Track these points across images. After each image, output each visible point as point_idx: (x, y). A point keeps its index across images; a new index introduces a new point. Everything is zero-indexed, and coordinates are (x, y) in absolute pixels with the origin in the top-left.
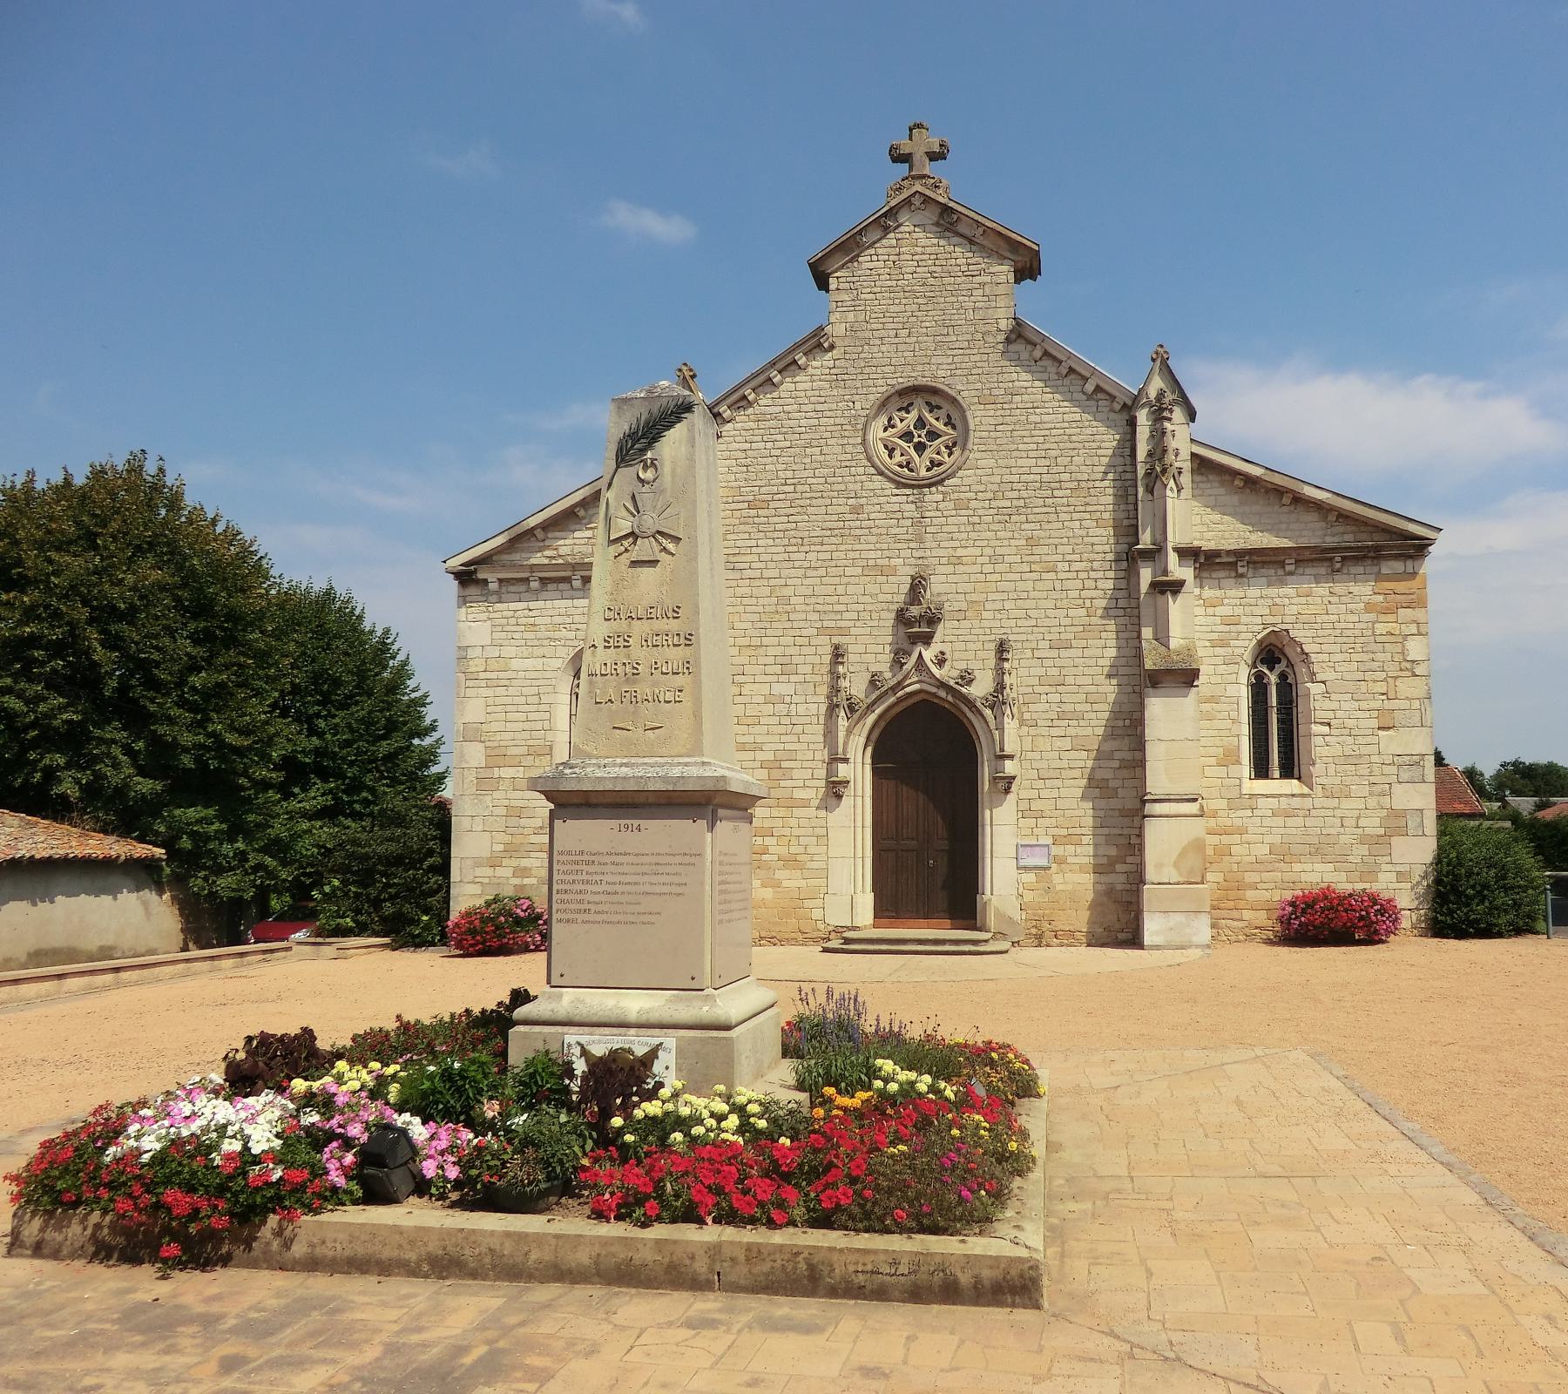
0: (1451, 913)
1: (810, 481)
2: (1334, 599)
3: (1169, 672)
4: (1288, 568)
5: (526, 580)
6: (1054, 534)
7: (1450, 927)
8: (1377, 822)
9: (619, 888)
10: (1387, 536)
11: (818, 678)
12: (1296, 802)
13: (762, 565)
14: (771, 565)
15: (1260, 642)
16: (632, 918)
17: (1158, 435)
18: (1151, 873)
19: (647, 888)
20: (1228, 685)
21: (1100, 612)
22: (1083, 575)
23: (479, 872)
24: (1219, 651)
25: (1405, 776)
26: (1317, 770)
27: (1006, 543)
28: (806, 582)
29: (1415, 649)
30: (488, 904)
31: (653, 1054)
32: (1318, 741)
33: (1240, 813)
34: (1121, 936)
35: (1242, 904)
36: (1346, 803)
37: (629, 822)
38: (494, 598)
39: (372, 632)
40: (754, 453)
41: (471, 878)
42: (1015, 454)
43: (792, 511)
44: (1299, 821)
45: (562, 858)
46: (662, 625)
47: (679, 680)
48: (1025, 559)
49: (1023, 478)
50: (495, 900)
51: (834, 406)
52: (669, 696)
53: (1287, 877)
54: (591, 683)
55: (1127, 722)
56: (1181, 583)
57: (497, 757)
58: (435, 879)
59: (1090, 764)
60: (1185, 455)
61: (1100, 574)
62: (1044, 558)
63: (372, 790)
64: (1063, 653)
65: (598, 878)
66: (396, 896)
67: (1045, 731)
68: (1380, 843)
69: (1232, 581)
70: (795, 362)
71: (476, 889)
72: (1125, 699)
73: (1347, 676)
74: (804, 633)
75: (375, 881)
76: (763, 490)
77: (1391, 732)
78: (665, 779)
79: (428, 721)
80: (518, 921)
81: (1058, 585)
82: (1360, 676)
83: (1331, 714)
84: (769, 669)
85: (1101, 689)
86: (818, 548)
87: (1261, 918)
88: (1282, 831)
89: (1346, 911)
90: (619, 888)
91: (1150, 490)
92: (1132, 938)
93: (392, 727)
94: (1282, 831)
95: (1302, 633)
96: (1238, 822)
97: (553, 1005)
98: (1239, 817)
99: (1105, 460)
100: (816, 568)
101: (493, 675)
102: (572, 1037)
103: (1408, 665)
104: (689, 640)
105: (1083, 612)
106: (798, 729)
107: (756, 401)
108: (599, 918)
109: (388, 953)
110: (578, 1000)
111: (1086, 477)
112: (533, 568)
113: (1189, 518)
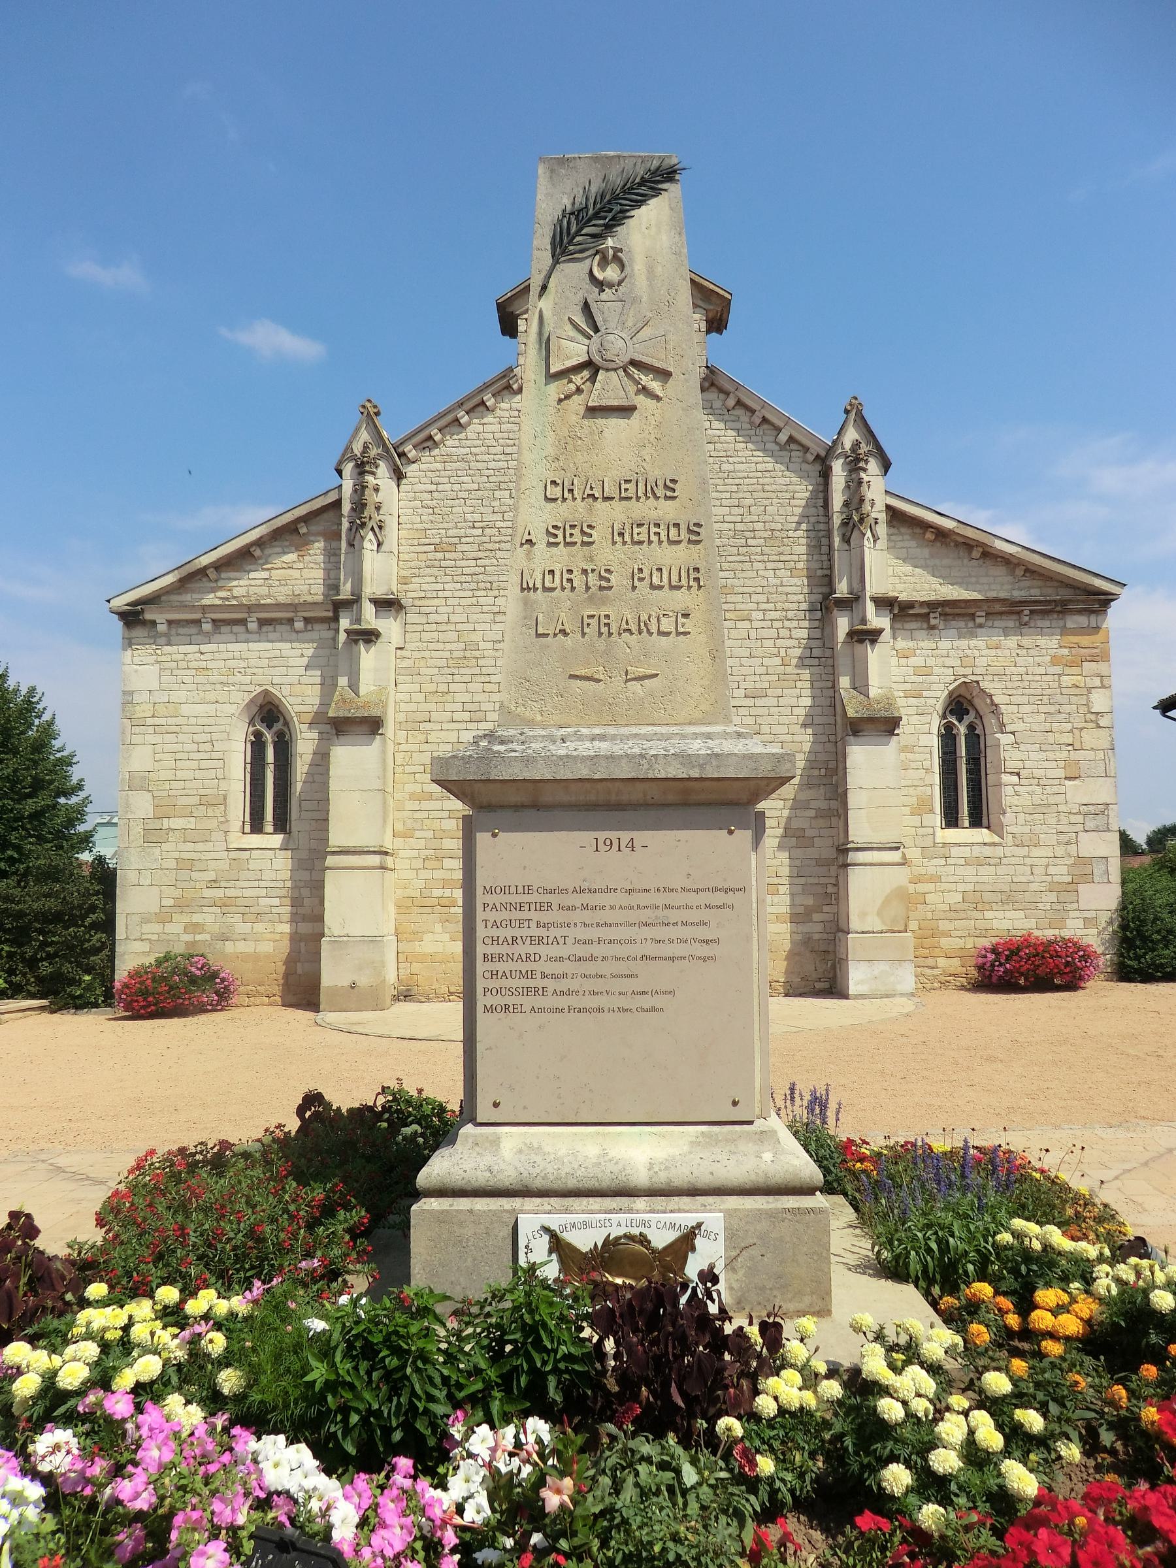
0: (1137, 958)
1: (499, 524)
2: (1023, 652)
3: (871, 720)
4: (979, 620)
5: (198, 622)
7: (1136, 971)
8: (1064, 870)
9: (597, 950)
10: (1072, 591)
12: (988, 851)
13: (450, 609)
14: (458, 609)
15: (951, 693)
17: (855, 485)
18: (855, 923)
19: (651, 949)
20: (922, 733)
21: (794, 661)
22: (777, 624)
23: (147, 928)
24: (912, 701)
25: (1090, 825)
26: (1007, 819)
28: (495, 627)
29: (1099, 701)
30: (159, 963)
31: (687, 1242)
32: (1009, 790)
33: (935, 862)
34: (819, 985)
35: (937, 952)
36: (1036, 852)
37: (613, 835)
38: (163, 640)
39: (16, 691)
40: (441, 495)
41: (137, 935)
43: (481, 554)
44: (992, 869)
45: (490, 899)
47: (681, 599)
50: (167, 958)
53: (981, 924)
55: (823, 772)
56: (879, 632)
57: (165, 808)
58: (98, 937)
59: (786, 813)
60: (880, 506)
61: (795, 624)
62: (739, 607)
63: (18, 848)
66: (56, 955)
69: (924, 632)
70: (483, 403)
71: (144, 947)
72: (820, 748)
73: (1035, 727)
74: (493, 679)
75: (31, 939)
76: (450, 533)
77: (1077, 782)
78: (684, 758)
79: (74, 781)
80: (193, 980)
81: (753, 633)
82: (1048, 727)
84: (456, 716)
85: (796, 738)
87: (954, 965)
88: (975, 879)
89: (1051, 957)
90: (597, 950)
91: (846, 540)
92: (831, 986)
93: (38, 785)
94: (975, 879)
95: (992, 685)
96: (932, 870)
97: (488, 1159)
98: (934, 866)
99: (798, 511)
102: (533, 1219)
103: (1093, 717)
105: (778, 661)
107: (442, 441)
108: (563, 1002)
109: (46, 1017)
110: (530, 1147)
111: (780, 526)
112: (205, 609)
113: (886, 570)
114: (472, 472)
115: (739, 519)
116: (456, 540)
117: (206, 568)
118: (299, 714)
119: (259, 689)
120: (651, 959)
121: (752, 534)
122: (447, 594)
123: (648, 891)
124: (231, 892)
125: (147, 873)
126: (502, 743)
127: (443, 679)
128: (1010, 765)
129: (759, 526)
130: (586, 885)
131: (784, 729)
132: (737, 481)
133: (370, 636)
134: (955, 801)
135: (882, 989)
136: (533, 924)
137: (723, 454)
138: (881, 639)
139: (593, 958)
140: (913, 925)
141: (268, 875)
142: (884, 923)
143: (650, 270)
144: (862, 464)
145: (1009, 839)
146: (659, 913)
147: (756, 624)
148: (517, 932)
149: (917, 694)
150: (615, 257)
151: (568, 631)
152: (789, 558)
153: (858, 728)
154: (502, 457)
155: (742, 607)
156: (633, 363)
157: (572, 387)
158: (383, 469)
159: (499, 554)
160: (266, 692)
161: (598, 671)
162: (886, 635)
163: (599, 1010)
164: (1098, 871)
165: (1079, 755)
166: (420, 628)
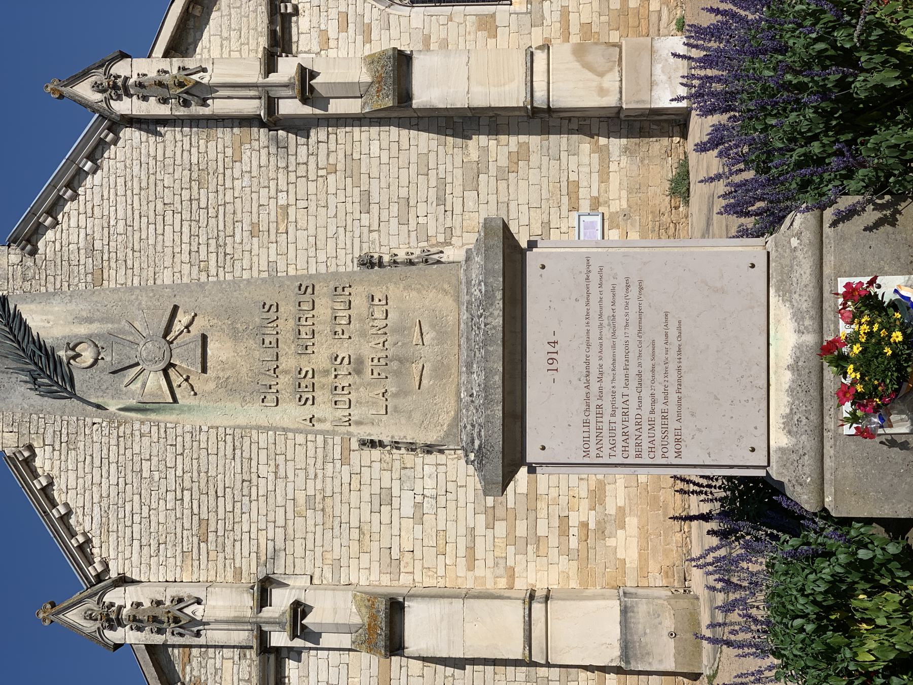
6: (247, 208)
9: (633, 371)
11: (397, 464)
13: (271, 525)
14: (271, 517)
16: (673, 353)
17: (143, 89)
18: (610, 101)
19: (633, 330)
24: (375, 35)
27: (255, 259)
33: (547, 14)
42: (159, 248)
46: (286, 326)
47: (359, 303)
48: (273, 238)
49: (186, 239)
51: (97, 446)
52: (379, 314)
54: (359, 423)
56: (302, 70)
60: (165, 64)
62: (273, 217)
64: (375, 198)
65: (619, 399)
67: (458, 219)
74: (346, 479)
76: (187, 525)
81: (302, 204)
86: (254, 463)
90: (633, 371)
96: (556, 16)
100: (277, 466)
104: (306, 288)
105: (331, 178)
106: (451, 487)
108: (673, 397)
111: (187, 173)
114: (120, 502)
115: (177, 216)
116: (196, 518)
120: (640, 330)
121: (195, 203)
123: (588, 331)
126: (473, 442)
127: (345, 534)
129: (186, 194)
130: (584, 379)
131: (404, 172)
132: (137, 216)
133: (299, 610)
136: (613, 419)
137: (106, 230)
138: (308, 66)
139: (639, 374)
140: (614, 37)
142: (611, 69)
143: (89, 320)
144: (119, 82)
146: (605, 322)
147: (292, 200)
148: (619, 432)
149: (366, 32)
150: (73, 349)
151: (384, 390)
152: (220, 164)
153: (404, 96)
155: (273, 214)
156: (165, 337)
157: (185, 384)
158: (115, 596)
159: (212, 473)
161: (415, 369)
162: (304, 59)
163: (679, 369)
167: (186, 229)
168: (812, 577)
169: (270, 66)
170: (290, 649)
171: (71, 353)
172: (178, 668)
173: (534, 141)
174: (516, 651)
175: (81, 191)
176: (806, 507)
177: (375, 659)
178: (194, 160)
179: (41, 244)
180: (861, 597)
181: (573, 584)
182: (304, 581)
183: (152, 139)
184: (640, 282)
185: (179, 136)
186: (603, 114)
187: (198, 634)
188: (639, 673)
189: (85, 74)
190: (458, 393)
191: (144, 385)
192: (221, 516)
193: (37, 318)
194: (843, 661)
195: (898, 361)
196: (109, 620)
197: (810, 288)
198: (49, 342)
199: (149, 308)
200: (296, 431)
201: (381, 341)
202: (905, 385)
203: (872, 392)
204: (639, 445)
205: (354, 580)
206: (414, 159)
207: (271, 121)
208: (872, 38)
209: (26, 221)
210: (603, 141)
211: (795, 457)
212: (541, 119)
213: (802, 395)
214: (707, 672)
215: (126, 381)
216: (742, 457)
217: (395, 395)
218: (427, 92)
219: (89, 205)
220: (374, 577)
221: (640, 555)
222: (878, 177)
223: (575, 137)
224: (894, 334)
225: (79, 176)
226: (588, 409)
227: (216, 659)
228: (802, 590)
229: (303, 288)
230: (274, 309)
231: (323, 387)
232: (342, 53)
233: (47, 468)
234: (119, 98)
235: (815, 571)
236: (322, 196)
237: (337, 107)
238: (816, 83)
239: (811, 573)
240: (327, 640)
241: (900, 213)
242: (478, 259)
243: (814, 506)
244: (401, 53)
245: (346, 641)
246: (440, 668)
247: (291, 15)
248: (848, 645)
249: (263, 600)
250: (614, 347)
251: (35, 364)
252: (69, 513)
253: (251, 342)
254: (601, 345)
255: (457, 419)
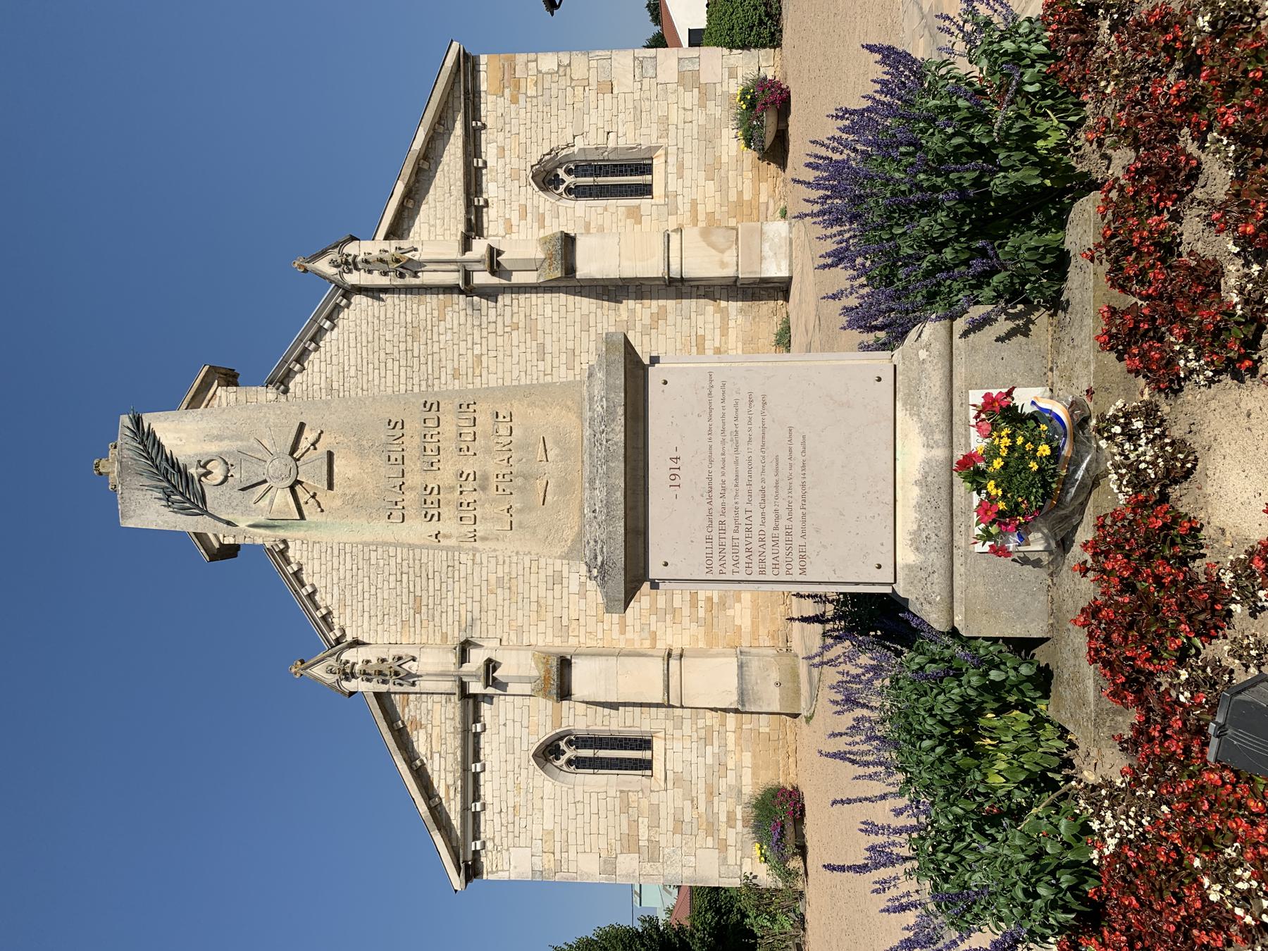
1: (399, 560)
2: (507, 127)
6: (450, 356)
9: (756, 488)
14: (469, 595)
15: (541, 189)
17: (367, 265)
18: (730, 272)
19: (756, 445)
20: (571, 214)
22: (485, 333)
23: (731, 861)
25: (651, 72)
33: (680, 206)
36: (673, 118)
44: (687, 157)
46: (412, 443)
47: (484, 419)
49: (403, 381)
52: (504, 431)
54: (484, 539)
56: (491, 249)
57: (630, 843)
60: (385, 245)
61: (484, 319)
62: (470, 364)
64: (548, 349)
65: (742, 516)
68: (705, 92)
73: (570, 118)
74: (527, 565)
76: (405, 601)
81: (492, 354)
83: (601, 131)
90: (756, 488)
94: (695, 171)
96: (688, 207)
98: (684, 206)
101: (558, 845)
103: (562, 69)
105: (515, 333)
108: (797, 513)
111: (403, 329)
115: (396, 363)
117: (430, 808)
118: (553, 728)
119: (532, 762)
122: (456, 604)
124: (702, 785)
125: (685, 860)
126: (596, 558)
127: (527, 607)
128: (601, 140)
129: (402, 346)
133: (491, 665)
134: (622, 174)
135: (785, 249)
136: (736, 535)
139: (763, 490)
140: (732, 222)
141: (687, 756)
142: (730, 247)
143: (220, 438)
144: (350, 259)
145: (662, 141)
146: (728, 438)
147: (485, 352)
148: (742, 548)
150: (204, 467)
153: (570, 269)
154: (342, 557)
155: (470, 361)
156: (291, 454)
160: (535, 756)
161: (540, 485)
163: (803, 485)
164: (688, 66)
165: (593, 81)
166: (484, 626)
167: (403, 373)
168: (941, 698)
169: (466, 246)
170: (485, 695)
171: (202, 471)
172: (399, 710)
173: (670, 304)
174: (658, 697)
175: (322, 344)
176: (936, 626)
177: (550, 703)
178: (409, 320)
179: (291, 385)
180: (990, 715)
181: (701, 645)
182: (496, 643)
183: (376, 303)
184: (764, 396)
185: (397, 301)
186: (723, 282)
187: (413, 684)
188: (752, 713)
189: (324, 253)
190: (582, 509)
191: (272, 502)
192: (431, 593)
193: (170, 435)
194: (972, 783)
195: (1043, 477)
196: (345, 674)
197: (940, 401)
198: (182, 461)
199: (276, 426)
200: (421, 547)
201: (506, 457)
202: (1048, 502)
203: (1014, 510)
204: (762, 561)
205: (533, 642)
206: (578, 319)
207: (467, 289)
208: (1013, 131)
209: (280, 367)
210: (723, 304)
211: (923, 574)
212: (677, 287)
213: (931, 512)
214: (805, 713)
215: (255, 498)
216: (867, 576)
217: (520, 511)
218: (587, 267)
219: (328, 355)
220: (549, 639)
221: (753, 622)
222: (1012, 284)
223: (702, 301)
224: (1040, 448)
225: (321, 331)
226: (710, 526)
227: (428, 702)
228: (930, 711)
229: (428, 405)
230: (399, 426)
231: (448, 503)
232: (523, 236)
233: (298, 557)
234: (350, 271)
235: (943, 690)
236: (508, 348)
237: (518, 278)
238: (951, 182)
239: (939, 694)
240: (512, 688)
241: (1033, 323)
242: (600, 375)
243: (944, 625)
244: (567, 235)
245: (527, 688)
246: (600, 709)
247: (483, 207)
248: (978, 767)
249: (463, 658)
250: (736, 462)
251: (169, 481)
252: (314, 592)
253: (377, 458)
254: (724, 460)
255: (581, 534)
